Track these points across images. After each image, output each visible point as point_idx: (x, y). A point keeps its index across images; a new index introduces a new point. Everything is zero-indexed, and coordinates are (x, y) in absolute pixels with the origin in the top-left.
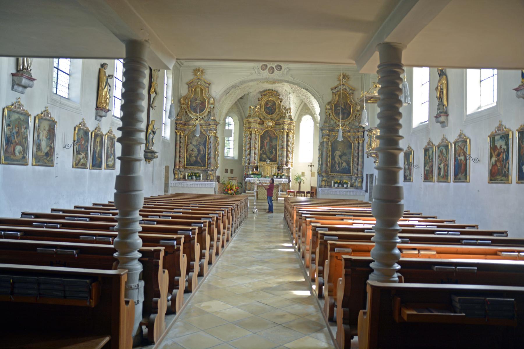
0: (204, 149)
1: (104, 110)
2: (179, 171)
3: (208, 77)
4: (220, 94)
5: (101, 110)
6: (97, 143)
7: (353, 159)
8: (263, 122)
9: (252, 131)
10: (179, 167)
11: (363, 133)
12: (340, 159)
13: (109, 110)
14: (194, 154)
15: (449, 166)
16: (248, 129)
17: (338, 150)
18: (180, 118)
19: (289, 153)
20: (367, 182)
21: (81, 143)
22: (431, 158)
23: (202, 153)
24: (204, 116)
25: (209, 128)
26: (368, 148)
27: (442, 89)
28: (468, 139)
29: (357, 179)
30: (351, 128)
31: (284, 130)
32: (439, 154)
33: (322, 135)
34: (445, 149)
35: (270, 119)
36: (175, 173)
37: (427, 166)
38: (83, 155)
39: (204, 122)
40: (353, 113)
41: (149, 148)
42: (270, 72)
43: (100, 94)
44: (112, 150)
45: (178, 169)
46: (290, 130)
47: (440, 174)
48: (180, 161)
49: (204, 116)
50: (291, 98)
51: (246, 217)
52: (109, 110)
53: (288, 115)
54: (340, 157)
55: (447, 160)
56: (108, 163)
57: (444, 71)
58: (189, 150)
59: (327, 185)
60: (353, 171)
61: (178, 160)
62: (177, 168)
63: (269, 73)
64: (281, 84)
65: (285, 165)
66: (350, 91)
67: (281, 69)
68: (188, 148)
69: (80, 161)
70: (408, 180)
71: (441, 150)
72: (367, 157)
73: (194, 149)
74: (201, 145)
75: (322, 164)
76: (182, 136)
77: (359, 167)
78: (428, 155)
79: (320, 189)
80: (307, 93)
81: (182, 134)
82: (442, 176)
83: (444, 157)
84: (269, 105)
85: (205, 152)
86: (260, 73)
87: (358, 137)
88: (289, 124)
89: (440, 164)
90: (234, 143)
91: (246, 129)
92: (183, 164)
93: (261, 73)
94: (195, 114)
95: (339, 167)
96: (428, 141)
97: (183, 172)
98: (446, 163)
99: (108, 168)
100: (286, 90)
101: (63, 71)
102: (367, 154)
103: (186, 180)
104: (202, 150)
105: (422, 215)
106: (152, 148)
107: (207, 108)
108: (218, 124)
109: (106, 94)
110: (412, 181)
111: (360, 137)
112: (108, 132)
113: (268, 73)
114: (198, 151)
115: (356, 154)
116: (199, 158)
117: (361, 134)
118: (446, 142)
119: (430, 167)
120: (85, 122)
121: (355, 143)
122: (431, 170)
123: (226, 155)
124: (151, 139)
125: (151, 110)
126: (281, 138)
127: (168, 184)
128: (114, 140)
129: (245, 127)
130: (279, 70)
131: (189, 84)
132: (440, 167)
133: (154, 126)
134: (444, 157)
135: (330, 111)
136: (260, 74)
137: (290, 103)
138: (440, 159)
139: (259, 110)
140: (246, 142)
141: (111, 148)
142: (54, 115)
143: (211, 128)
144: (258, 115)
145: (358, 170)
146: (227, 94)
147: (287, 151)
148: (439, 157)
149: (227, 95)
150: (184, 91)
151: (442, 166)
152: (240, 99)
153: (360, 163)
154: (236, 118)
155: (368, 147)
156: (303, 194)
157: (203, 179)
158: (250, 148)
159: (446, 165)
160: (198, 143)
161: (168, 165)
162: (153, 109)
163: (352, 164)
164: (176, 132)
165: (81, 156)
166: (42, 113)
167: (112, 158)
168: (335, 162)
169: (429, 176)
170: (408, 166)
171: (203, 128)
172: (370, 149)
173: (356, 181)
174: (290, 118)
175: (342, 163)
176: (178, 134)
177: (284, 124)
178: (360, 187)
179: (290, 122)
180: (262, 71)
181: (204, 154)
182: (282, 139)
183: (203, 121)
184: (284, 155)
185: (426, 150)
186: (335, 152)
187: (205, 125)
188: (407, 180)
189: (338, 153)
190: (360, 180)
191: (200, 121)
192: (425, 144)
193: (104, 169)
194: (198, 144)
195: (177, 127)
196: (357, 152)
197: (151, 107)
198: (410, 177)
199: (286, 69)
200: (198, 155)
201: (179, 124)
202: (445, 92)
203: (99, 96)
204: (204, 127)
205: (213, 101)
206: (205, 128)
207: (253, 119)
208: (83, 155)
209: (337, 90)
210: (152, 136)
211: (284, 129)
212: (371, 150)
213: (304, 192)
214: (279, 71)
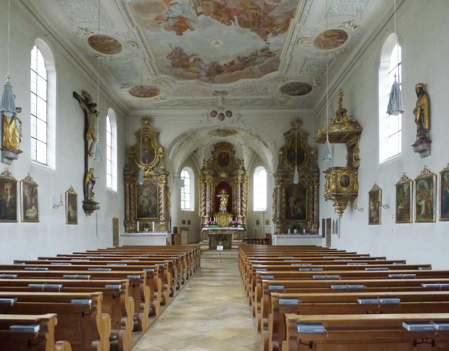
0: (155, 200)
1: (12, 150)
2: (129, 223)
3: (157, 124)
4: (169, 143)
5: (8, 150)
6: (5, 191)
7: (308, 205)
8: (217, 174)
9: (207, 183)
10: (130, 219)
11: (318, 178)
12: (294, 205)
13: (20, 152)
15: (434, 202)
16: (203, 181)
17: (293, 195)
18: (128, 169)
19: (243, 203)
20: (323, 228)
22: (406, 195)
23: (153, 204)
24: (154, 166)
25: (159, 179)
26: (326, 191)
27: (422, 110)
28: (435, 175)
29: (313, 225)
30: (305, 174)
31: (238, 181)
32: (418, 189)
33: (276, 182)
34: (427, 183)
35: (224, 171)
36: (126, 225)
37: (401, 205)
39: (154, 172)
40: (307, 157)
41: (88, 198)
42: (220, 119)
43: (5, 131)
44: (33, 199)
45: (129, 221)
46: (244, 180)
47: (421, 213)
49: (153, 167)
50: (244, 149)
52: (20, 152)
53: (241, 166)
54: (295, 203)
55: (430, 195)
56: (27, 215)
58: (140, 202)
59: (282, 231)
60: (308, 217)
61: (128, 212)
62: (127, 220)
63: (219, 120)
64: (233, 136)
65: (240, 215)
66: (304, 136)
67: (231, 116)
68: (138, 199)
70: (375, 222)
71: (422, 184)
72: (325, 200)
73: (144, 201)
74: (152, 196)
75: (276, 211)
76: (132, 188)
77: (315, 213)
78: (401, 192)
79: (275, 235)
81: (132, 186)
82: (422, 215)
83: (426, 192)
84: (223, 158)
85: (156, 203)
86: (210, 120)
87: (313, 182)
88: (243, 175)
89: (420, 201)
90: (190, 195)
91: (200, 181)
92: (134, 216)
93: (211, 120)
94: (143, 164)
95: (294, 213)
96: (402, 176)
97: (134, 224)
99: (28, 220)
102: (326, 197)
103: (138, 232)
104: (153, 201)
105: (386, 259)
106: (92, 198)
107: (156, 158)
108: (168, 174)
109: (14, 131)
110: (380, 223)
111: (315, 182)
112: (69, 190)
113: (218, 120)
114: (149, 202)
115: (311, 200)
116: (150, 209)
118: (429, 173)
119: (404, 206)
120: (31, 177)
121: (310, 188)
122: (407, 209)
123: (182, 207)
124: (90, 188)
125: (90, 159)
126: (235, 189)
127: (118, 236)
129: (200, 179)
130: (229, 116)
131: (138, 134)
133: (93, 174)
134: (426, 192)
135: (283, 157)
136: (210, 121)
137: (242, 155)
139: (212, 163)
140: (201, 193)
142: (35, 180)
143: (161, 178)
144: (212, 167)
145: (313, 215)
146: (180, 146)
147: (242, 201)
148: (417, 192)
150: (132, 141)
151: (423, 203)
152: (194, 153)
153: (315, 208)
154: (191, 170)
155: (326, 190)
156: (258, 242)
157: (155, 230)
160: (148, 194)
161: (116, 217)
162: (90, 157)
163: (307, 210)
164: (125, 183)
166: (3, 174)
168: (290, 208)
171: (153, 179)
172: (329, 191)
173: (312, 227)
174: (243, 169)
175: (297, 209)
176: (127, 185)
177: (238, 175)
178: (316, 232)
179: (243, 173)
180: (211, 118)
181: (155, 205)
182: (236, 190)
183: (152, 171)
184: (239, 205)
185: (399, 187)
186: (289, 198)
187: (155, 176)
188: (373, 222)
189: (292, 199)
190: (316, 226)
191: (150, 172)
192: (397, 179)
194: (149, 195)
195: (126, 178)
196: (312, 197)
197: (89, 155)
198: (377, 219)
199: (236, 115)
200: (149, 207)
201: (128, 175)
202: (426, 114)
203: (4, 133)
204: (154, 177)
205: (162, 150)
206: (155, 179)
207: (207, 171)
209: (289, 135)
210: (91, 186)
211: (237, 180)
212: (330, 192)
213: (259, 240)
214: (229, 117)
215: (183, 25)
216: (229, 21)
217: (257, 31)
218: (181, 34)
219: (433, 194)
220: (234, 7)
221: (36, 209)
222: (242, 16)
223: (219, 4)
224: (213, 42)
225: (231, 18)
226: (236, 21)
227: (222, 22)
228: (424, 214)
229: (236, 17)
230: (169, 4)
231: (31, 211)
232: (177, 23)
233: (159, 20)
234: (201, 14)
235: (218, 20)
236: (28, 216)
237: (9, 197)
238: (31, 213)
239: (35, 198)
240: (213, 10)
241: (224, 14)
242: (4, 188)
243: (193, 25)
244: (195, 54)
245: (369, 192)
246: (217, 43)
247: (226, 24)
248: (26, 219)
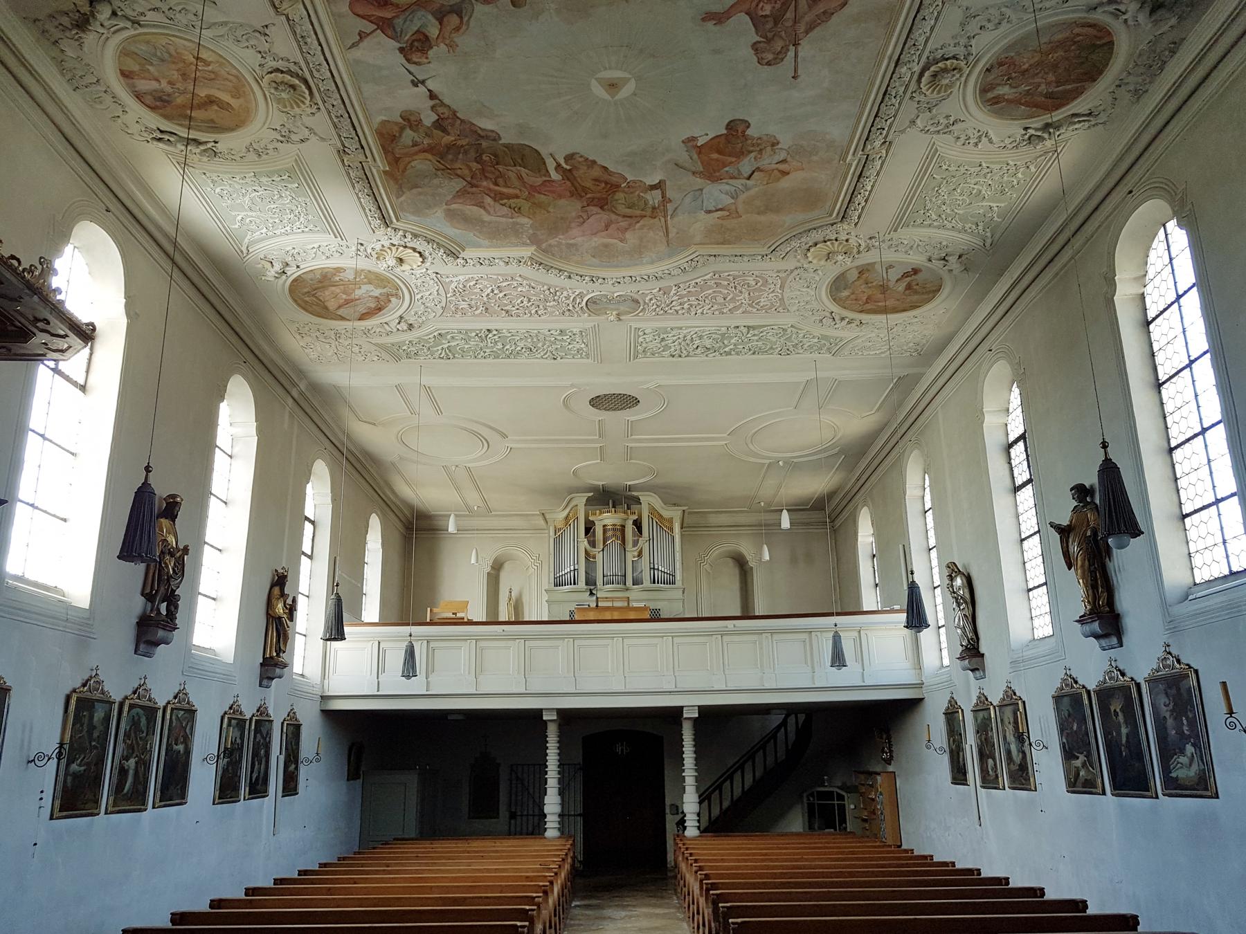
21: (1072, 728)
22: (96, 734)
37: (78, 761)
38: (1082, 758)
44: (1185, 722)
56: (1174, 775)
69: (1079, 774)
78: (86, 721)
98: (143, 757)
101: (1214, 422)
128: (1184, 685)
132: (126, 768)
138: (129, 742)
141: (1177, 719)
151: (132, 762)
159: (144, 765)
165: (1078, 763)
167: (1189, 755)
193: (244, 800)
208: (1082, 758)
215: (715, 156)
216: (572, 168)
217: (479, 135)
218: (731, 126)
219: (151, 747)
220: (562, 202)
221: (1198, 750)
222: (539, 181)
223: (602, 208)
224: (626, 92)
225: (568, 175)
226: (551, 165)
227: (594, 162)
228: (130, 792)
229: (555, 176)
230: (728, 211)
231: (1184, 760)
232: (731, 163)
233: (779, 171)
234: (653, 187)
235: (605, 168)
236: (1177, 779)
237: (1124, 731)
238: (1185, 770)
239: (1190, 716)
240: (620, 196)
241: (589, 184)
242: (1110, 709)
243: (683, 156)
244: (710, 25)
245: (8, 690)
246: (613, 86)
247: (580, 159)
248: (1175, 787)
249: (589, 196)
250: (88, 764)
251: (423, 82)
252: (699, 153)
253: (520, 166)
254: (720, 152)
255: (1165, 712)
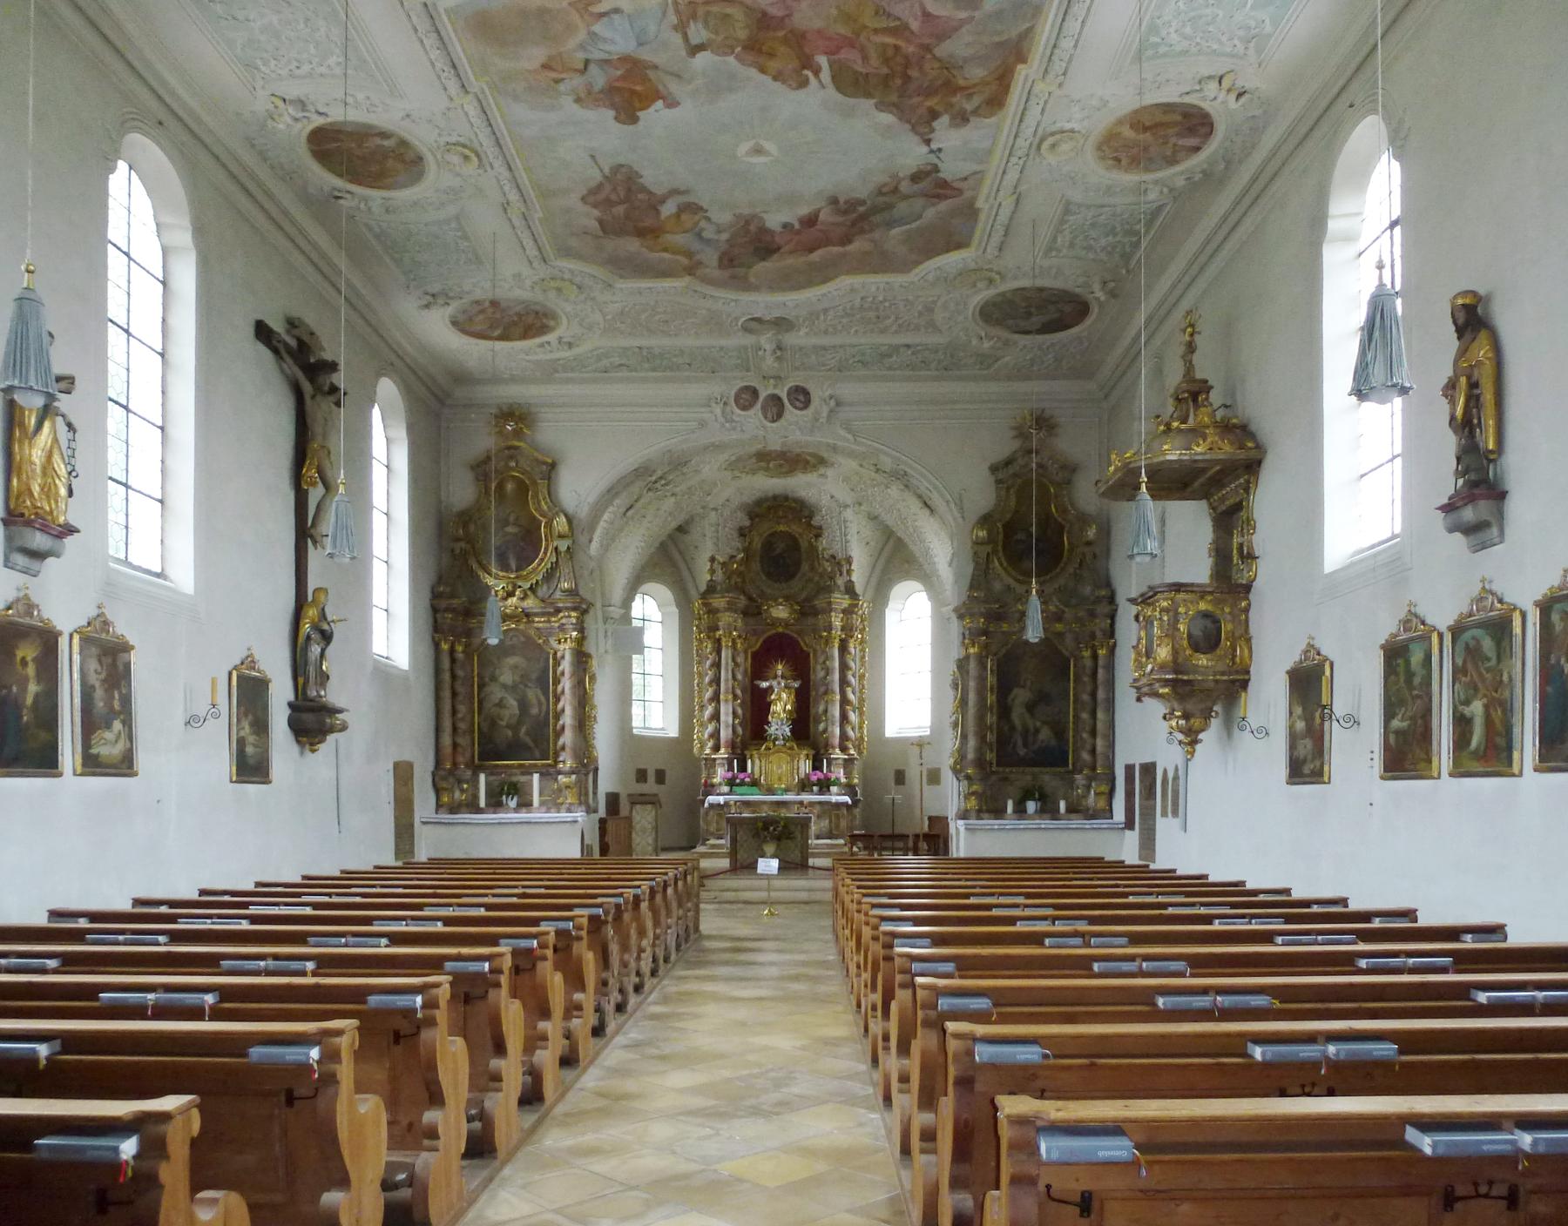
0: (543, 698)
1: (42, 525)
4: (591, 499)
5: (29, 524)
6: (19, 667)
7: (1076, 717)
8: (759, 607)
9: (724, 639)
10: (455, 764)
11: (1109, 621)
12: (1027, 716)
13: (70, 530)
14: (506, 719)
15: (1517, 705)
16: (710, 632)
17: (1022, 682)
18: (448, 590)
19: (848, 707)
20: (1130, 795)
22: (1417, 681)
23: (535, 711)
24: (537, 581)
25: (557, 625)
26: (1140, 666)
27: (1474, 385)
28: (1518, 612)
29: (1093, 784)
31: (829, 633)
32: (1459, 662)
33: (964, 634)
34: (1493, 638)
35: (783, 597)
36: (439, 786)
37: (1400, 716)
39: (537, 601)
40: (1071, 550)
42: (769, 415)
43: (18, 458)
44: (117, 696)
45: (451, 772)
47: (1469, 743)
48: (455, 745)
49: (534, 582)
50: (851, 522)
51: (692, 937)
52: (70, 530)
53: (840, 581)
54: (1031, 708)
55: (1501, 681)
56: (94, 751)
57: (1479, 310)
58: (487, 705)
59: (984, 808)
60: (1077, 758)
61: (447, 740)
62: (444, 769)
63: (766, 418)
64: (815, 474)
65: (837, 751)
66: (1060, 475)
67: (807, 404)
68: (483, 695)
70: (1309, 776)
71: (1472, 644)
72: (1134, 699)
74: (529, 685)
75: (964, 737)
76: (460, 656)
78: (1401, 669)
79: (961, 822)
80: (904, 504)
81: (459, 648)
82: (1475, 753)
83: (1488, 670)
84: (778, 551)
85: (544, 708)
86: (733, 421)
87: (1093, 636)
88: (848, 612)
89: (1467, 703)
90: (664, 681)
91: (700, 633)
92: (468, 755)
93: (737, 419)
95: (1025, 745)
96: (1402, 615)
97: (467, 783)
99: (98, 770)
100: (832, 497)
102: (1138, 688)
103: (482, 809)
105: (1346, 906)
106: (323, 693)
107: (545, 553)
109: (49, 456)
110: (1326, 779)
112: (242, 663)
113: (762, 418)
114: (519, 705)
115: (1086, 697)
116: (523, 730)
117: (1103, 625)
119: (1411, 718)
120: (110, 617)
121: (1083, 657)
123: (637, 722)
124: (313, 658)
125: (314, 557)
126: (821, 660)
127: (412, 825)
129: (697, 626)
130: (801, 405)
131: (481, 469)
133: (323, 609)
134: (1488, 670)
135: (989, 548)
136: (734, 424)
137: (847, 542)
139: (742, 568)
140: (701, 676)
142: (123, 627)
143: (564, 621)
145: (1093, 752)
146: (628, 510)
147: (844, 701)
148: (1457, 672)
149: (630, 513)
150: (461, 492)
151: (1477, 708)
152: (678, 533)
153: (1100, 726)
154: (666, 593)
156: (900, 844)
157: (542, 803)
158: (716, 698)
160: (517, 679)
161: (407, 757)
162: (316, 548)
163: (1071, 734)
166: (9, 608)
168: (1013, 728)
169: (1410, 756)
170: (1306, 720)
171: (536, 625)
172: (1150, 667)
173: (1089, 792)
174: (850, 590)
175: (1037, 731)
176: (445, 647)
177: (831, 610)
178: (1104, 810)
179: (850, 605)
180: (738, 411)
182: (824, 662)
184: (833, 716)
185: (1395, 653)
186: (1010, 690)
187: (543, 614)
188: (1301, 775)
189: (1020, 696)
190: (1104, 788)
192: (1387, 626)
194: (521, 683)
195: (439, 620)
196: (1089, 688)
197: (309, 541)
198: (1318, 763)
200: (520, 723)
202: (1488, 397)
203: (15, 465)
204: (537, 619)
205: (565, 524)
206: (541, 625)
207: (723, 597)
209: (1011, 471)
210: (319, 650)
211: (829, 628)
212: (1152, 670)
213: (904, 837)
214: (801, 409)
217: (898, 109)
218: (633, 120)
219: (1511, 679)
220: (818, 24)
221: (126, 728)
222: (844, 54)
223: (764, 14)
224: (744, 147)
225: (807, 63)
226: (825, 75)
227: (775, 79)
229: (822, 60)
230: (592, 14)
231: (108, 735)
232: (617, 80)
233: (554, 70)
234: (700, 48)
235: (763, 70)
236: (97, 756)
237: (33, 688)
238: (108, 746)
240: (742, 34)
241: (782, 49)
242: (15, 655)
243: (674, 87)
245: (1288, 672)
246: (758, 151)
248: (92, 765)
249: (781, 34)
250: (1411, 718)
251: (932, 151)
252: (657, 91)
253: (861, 73)
254: (633, 92)
255: (94, 679)
